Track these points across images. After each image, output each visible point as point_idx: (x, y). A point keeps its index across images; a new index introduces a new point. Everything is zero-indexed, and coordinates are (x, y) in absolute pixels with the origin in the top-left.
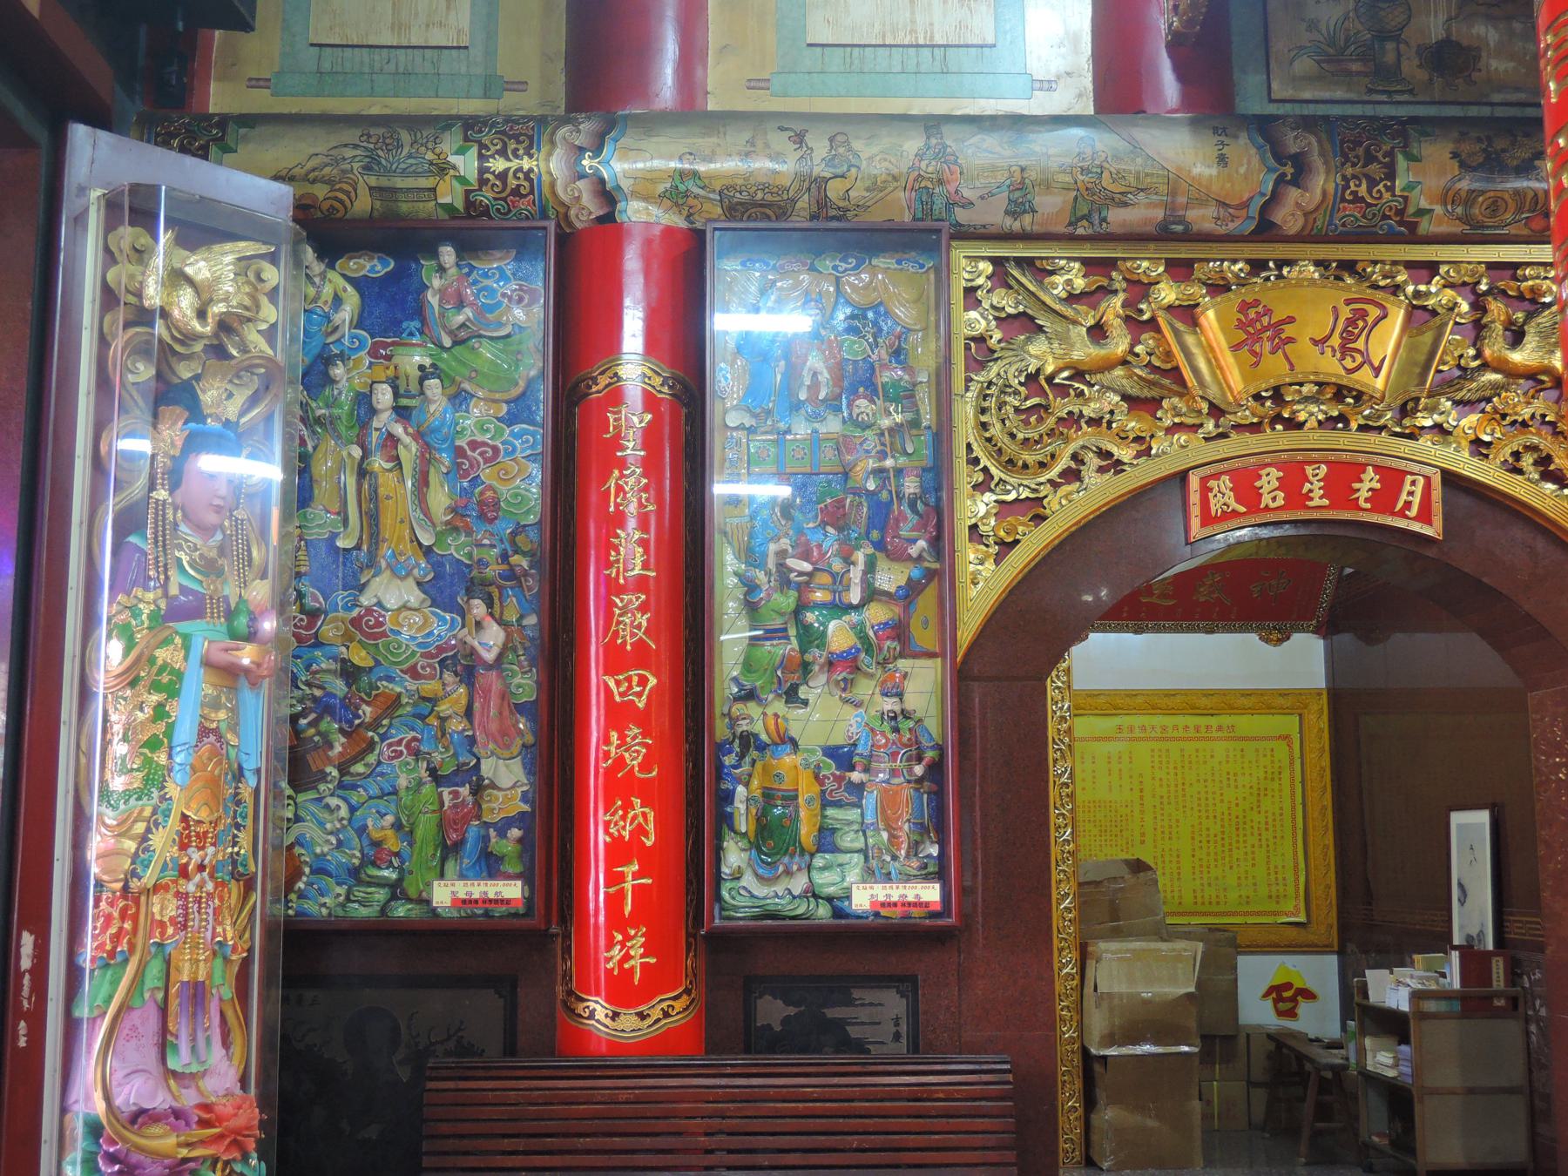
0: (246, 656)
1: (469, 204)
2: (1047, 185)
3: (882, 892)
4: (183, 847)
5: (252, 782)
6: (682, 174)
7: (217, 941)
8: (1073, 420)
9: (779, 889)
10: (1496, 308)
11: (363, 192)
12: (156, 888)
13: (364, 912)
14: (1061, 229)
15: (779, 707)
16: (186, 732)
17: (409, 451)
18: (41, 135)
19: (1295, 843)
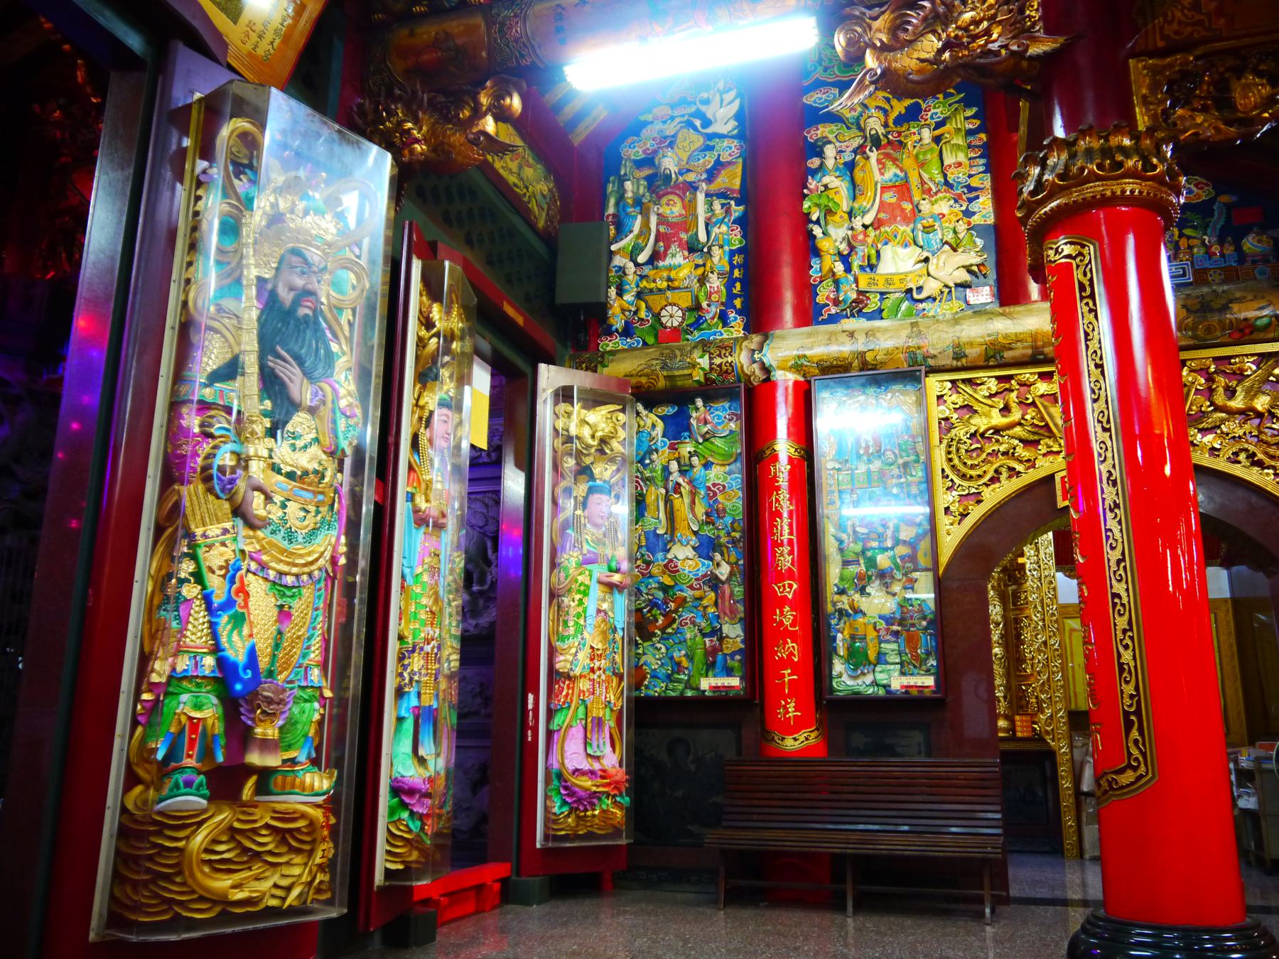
0: (616, 578)
1: (707, 379)
2: (971, 344)
3: (906, 681)
4: (592, 660)
5: (621, 633)
6: (799, 357)
7: (608, 699)
8: (994, 453)
9: (860, 682)
10: (1221, 380)
11: (661, 378)
12: (581, 676)
13: (673, 694)
14: (982, 363)
15: (857, 597)
16: (591, 611)
17: (686, 489)
18: (528, 370)
19: (134, 303)
